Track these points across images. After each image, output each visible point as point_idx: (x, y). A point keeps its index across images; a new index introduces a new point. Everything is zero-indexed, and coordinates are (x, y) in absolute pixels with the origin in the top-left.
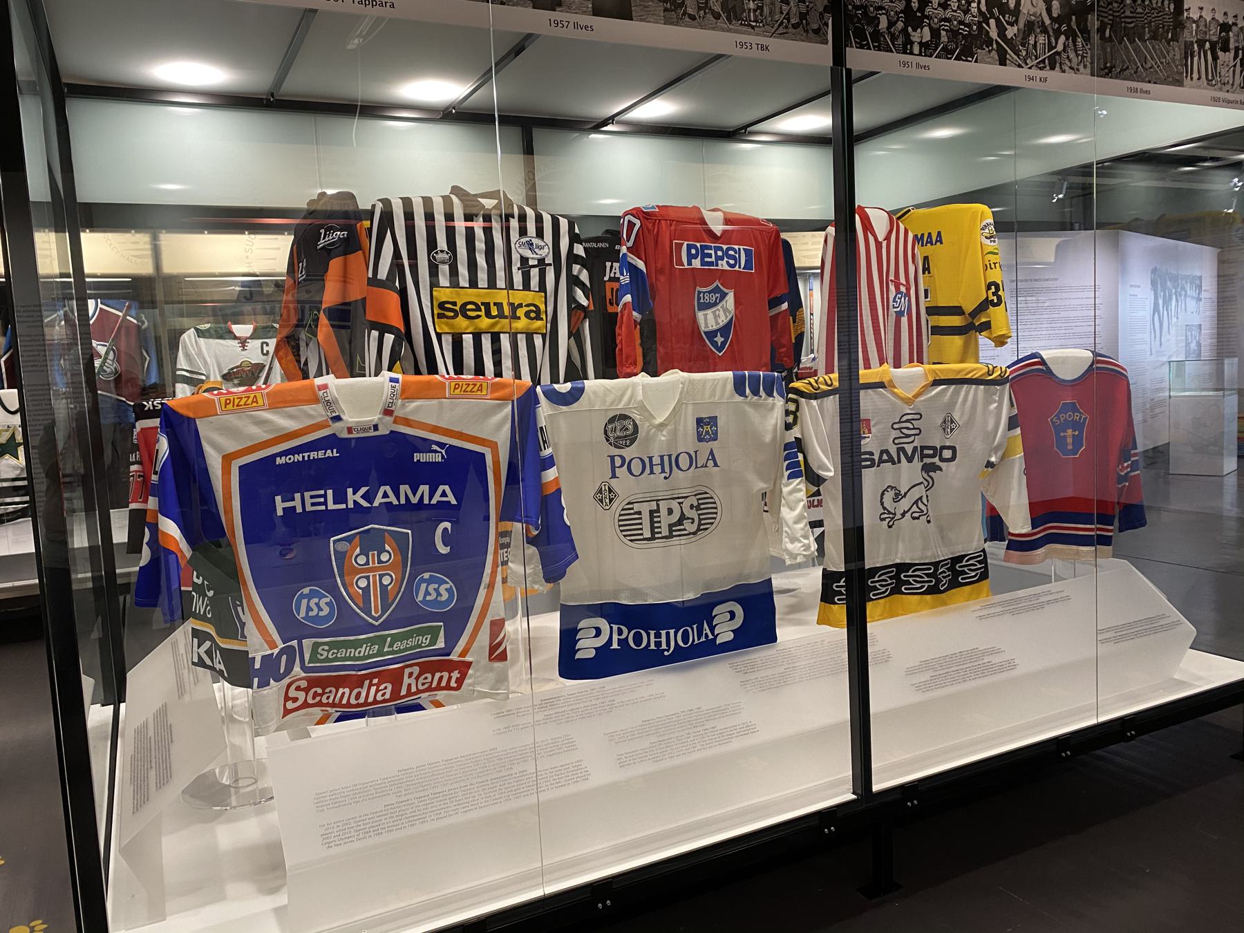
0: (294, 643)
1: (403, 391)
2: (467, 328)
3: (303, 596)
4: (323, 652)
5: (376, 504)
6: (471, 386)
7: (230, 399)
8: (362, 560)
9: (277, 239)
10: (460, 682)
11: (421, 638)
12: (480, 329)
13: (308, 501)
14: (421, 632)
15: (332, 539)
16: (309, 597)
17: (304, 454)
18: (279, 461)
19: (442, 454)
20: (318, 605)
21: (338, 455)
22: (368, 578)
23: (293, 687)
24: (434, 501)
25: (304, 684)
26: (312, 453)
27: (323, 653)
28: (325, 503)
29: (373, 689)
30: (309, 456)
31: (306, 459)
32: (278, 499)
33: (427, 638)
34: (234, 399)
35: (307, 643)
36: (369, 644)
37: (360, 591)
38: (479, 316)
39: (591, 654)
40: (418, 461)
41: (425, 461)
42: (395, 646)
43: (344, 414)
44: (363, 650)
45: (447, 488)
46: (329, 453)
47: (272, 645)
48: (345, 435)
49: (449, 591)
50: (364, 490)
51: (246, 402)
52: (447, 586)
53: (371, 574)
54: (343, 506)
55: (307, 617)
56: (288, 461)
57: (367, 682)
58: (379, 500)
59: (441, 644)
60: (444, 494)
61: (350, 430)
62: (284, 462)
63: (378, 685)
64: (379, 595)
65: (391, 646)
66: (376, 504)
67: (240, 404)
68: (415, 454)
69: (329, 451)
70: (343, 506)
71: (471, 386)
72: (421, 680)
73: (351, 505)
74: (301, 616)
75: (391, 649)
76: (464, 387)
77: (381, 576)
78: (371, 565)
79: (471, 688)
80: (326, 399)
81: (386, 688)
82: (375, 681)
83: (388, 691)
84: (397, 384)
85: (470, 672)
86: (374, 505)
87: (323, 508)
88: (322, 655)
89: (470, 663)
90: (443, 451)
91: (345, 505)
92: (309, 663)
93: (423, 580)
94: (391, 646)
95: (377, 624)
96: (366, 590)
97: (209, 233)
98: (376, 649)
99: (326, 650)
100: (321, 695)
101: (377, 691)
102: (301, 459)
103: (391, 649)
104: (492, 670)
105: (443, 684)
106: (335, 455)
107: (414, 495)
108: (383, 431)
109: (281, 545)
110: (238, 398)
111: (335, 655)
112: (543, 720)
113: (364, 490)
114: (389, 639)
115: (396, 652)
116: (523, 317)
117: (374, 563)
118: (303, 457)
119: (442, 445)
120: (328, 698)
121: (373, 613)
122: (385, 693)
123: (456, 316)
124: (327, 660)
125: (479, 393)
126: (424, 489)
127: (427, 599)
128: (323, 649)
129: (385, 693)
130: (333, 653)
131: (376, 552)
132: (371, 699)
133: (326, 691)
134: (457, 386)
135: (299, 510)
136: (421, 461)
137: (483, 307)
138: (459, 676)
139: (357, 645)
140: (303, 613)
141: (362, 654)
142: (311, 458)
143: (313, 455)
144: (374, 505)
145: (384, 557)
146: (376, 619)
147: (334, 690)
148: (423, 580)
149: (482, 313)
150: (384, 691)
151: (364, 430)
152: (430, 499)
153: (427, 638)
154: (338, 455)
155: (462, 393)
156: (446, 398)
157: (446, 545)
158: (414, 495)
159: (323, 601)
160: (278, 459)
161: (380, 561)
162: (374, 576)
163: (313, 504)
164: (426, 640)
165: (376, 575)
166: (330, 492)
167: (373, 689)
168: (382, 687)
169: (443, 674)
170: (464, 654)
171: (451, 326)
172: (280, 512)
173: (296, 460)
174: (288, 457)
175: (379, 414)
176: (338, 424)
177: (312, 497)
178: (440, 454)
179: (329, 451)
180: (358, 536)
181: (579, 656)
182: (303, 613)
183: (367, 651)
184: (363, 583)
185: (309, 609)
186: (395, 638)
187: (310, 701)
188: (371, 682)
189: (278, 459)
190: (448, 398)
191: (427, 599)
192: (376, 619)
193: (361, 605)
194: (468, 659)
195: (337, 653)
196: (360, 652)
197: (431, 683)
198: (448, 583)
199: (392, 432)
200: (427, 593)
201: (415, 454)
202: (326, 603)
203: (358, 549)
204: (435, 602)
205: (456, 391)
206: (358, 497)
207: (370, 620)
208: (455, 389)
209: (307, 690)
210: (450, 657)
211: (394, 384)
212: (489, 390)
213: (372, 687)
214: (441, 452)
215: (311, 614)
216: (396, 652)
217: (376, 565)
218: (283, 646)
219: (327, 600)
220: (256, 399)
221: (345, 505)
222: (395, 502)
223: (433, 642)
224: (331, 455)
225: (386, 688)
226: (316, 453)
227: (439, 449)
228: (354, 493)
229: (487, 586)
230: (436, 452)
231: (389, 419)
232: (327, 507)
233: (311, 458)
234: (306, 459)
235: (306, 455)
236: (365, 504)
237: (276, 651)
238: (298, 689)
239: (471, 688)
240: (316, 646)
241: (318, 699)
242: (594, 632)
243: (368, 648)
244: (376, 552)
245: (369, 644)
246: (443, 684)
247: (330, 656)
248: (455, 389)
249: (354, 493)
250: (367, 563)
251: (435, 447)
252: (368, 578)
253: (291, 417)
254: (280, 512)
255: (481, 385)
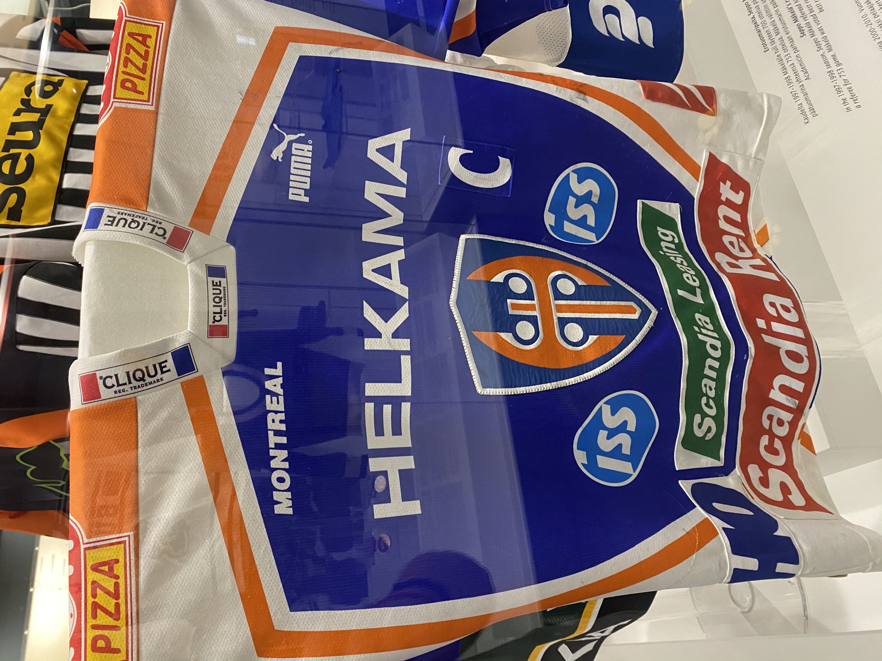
0: (686, 486)
1: (128, 202)
2: (50, 179)
3: (592, 464)
4: (705, 428)
5: (403, 291)
6: (133, 56)
7: (95, 640)
8: (526, 330)
9: (42, 558)
10: (740, 185)
11: (663, 244)
12: (57, 160)
13: (388, 441)
14: (654, 242)
15: (479, 390)
16: (593, 451)
17: (272, 445)
18: (284, 506)
19: (297, 141)
20: (612, 433)
21: (279, 364)
22: (563, 322)
23: (762, 490)
24: (402, 176)
25: (754, 471)
26: (270, 425)
27: (704, 428)
28: (396, 402)
29: (776, 327)
30: (277, 433)
31: (283, 440)
32: (380, 511)
33: (663, 234)
34: (95, 627)
35: (683, 460)
36: (696, 329)
37: (592, 338)
38: (30, 159)
39: (646, 25)
40: (307, 193)
41: (308, 180)
42: (691, 282)
43: (166, 342)
44: (710, 341)
45: (374, 144)
46: (275, 385)
47: (705, 532)
48: (229, 346)
49: (583, 176)
50: (369, 313)
51: (108, 593)
52: (573, 178)
53: (556, 315)
54: (406, 362)
55: (633, 459)
56: (287, 484)
57: (767, 339)
58: (396, 285)
59: (673, 210)
60: (387, 152)
61: (217, 331)
62: (289, 495)
63: (769, 319)
64: (598, 303)
65: (692, 290)
66: (403, 291)
67: (112, 609)
68: (291, 197)
69: (269, 385)
70: (406, 362)
71: (133, 56)
72: (736, 252)
73: (404, 344)
74: (630, 472)
75: (698, 291)
76: (132, 69)
77: (559, 296)
78: (536, 313)
79: (751, 164)
80: (123, 379)
81: (773, 305)
82: (761, 323)
83: (779, 301)
84: (107, 212)
85: (724, 160)
86: (406, 296)
87: (406, 407)
88: (709, 429)
89: (712, 159)
90: (289, 138)
91: (402, 357)
92: (719, 459)
93: (558, 227)
94: (692, 290)
95: (654, 313)
96: (589, 326)
97: (27, 628)
98: (704, 318)
99: (702, 420)
100: (772, 436)
101: (780, 320)
102: (284, 454)
103: (698, 291)
104: (728, 115)
105: (737, 217)
106: (279, 371)
107: (384, 215)
108: (228, 258)
109: (375, 550)
110: (95, 616)
111: (712, 403)
112: (813, 35)
113: (369, 313)
114: (680, 292)
115: (702, 280)
116: (49, 101)
117: (532, 307)
118: (278, 446)
119: (273, 139)
120: (780, 423)
121: (635, 316)
122: (783, 306)
123: (22, 194)
124: (718, 419)
125: (151, 42)
126: (373, 191)
127: (593, 225)
128: (700, 425)
129: (783, 306)
130: (708, 405)
131: (508, 301)
132: (799, 333)
133: (767, 427)
134: (128, 85)
135: (408, 462)
136: (307, 187)
137: (12, 151)
138: (729, 183)
139: (699, 352)
140: (625, 467)
141: (718, 344)
142: (283, 427)
143: (275, 422)
144: (406, 296)
145: (518, 286)
146: (646, 313)
147: (769, 410)
148: (558, 227)
149: (24, 153)
150: (779, 308)
151: (220, 298)
152: (396, 182)
153: (663, 234)
154: (279, 364)
155: (147, 76)
156: (156, 112)
157: (493, 167)
158: (384, 215)
159: (610, 421)
160: (279, 510)
161: (528, 295)
162: (559, 309)
163: (397, 430)
164: (667, 238)
165: (557, 305)
166: (372, 389)
167: (776, 327)
168: (772, 311)
169: (721, 215)
170: (693, 169)
171: (39, 203)
172: (414, 508)
173: (286, 465)
174: (276, 484)
175: (180, 258)
176: (200, 358)
177: (379, 432)
178: (295, 145)
179: (269, 385)
180: (475, 333)
181: (649, 40)
182: (625, 467)
183: (709, 333)
184: (575, 332)
185: (616, 453)
186: (677, 281)
187: (781, 460)
188: (762, 331)
189: (279, 510)
190: (157, 107)
191: (593, 225)
192: (646, 313)
193: (620, 338)
194: (702, 161)
195: (708, 398)
196: (714, 347)
197: (738, 236)
198: (568, 175)
199: (231, 239)
200: (582, 222)
201: (291, 197)
202: (613, 413)
203: (503, 335)
204: (601, 209)
205: (139, 89)
206: (387, 328)
207: (649, 324)
208: (134, 89)
209: (765, 466)
210: (696, 195)
211: (104, 219)
212: (146, 20)
213: (774, 329)
214: (290, 143)
215: (626, 450)
216: (702, 280)
217: (535, 302)
218: (698, 507)
219: (606, 410)
220: (104, 564)
221: (402, 357)
222: (401, 255)
223: (669, 223)
224: (280, 380)
225: (773, 305)
226: (270, 417)
227: (283, 146)
228: (378, 335)
229: (582, 96)
230: (288, 154)
231: (196, 240)
232: (404, 399)
233: (283, 427)
234: (283, 440)
235: (273, 440)
236: (402, 315)
237: (718, 524)
238: (765, 482)
239: (751, 164)
240: (693, 444)
241: (778, 444)
242: (610, 17)
243: (704, 331)
244: (508, 301)
245: (696, 329)
246: (737, 217)
247: (713, 412)
248: (134, 89)
249: (378, 335)
250: (533, 320)
251: (277, 153)
252: (563, 322)
253: (164, 473)
254: (414, 508)
255: (131, 35)
